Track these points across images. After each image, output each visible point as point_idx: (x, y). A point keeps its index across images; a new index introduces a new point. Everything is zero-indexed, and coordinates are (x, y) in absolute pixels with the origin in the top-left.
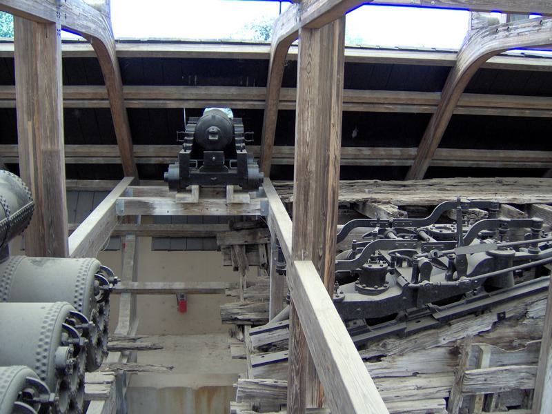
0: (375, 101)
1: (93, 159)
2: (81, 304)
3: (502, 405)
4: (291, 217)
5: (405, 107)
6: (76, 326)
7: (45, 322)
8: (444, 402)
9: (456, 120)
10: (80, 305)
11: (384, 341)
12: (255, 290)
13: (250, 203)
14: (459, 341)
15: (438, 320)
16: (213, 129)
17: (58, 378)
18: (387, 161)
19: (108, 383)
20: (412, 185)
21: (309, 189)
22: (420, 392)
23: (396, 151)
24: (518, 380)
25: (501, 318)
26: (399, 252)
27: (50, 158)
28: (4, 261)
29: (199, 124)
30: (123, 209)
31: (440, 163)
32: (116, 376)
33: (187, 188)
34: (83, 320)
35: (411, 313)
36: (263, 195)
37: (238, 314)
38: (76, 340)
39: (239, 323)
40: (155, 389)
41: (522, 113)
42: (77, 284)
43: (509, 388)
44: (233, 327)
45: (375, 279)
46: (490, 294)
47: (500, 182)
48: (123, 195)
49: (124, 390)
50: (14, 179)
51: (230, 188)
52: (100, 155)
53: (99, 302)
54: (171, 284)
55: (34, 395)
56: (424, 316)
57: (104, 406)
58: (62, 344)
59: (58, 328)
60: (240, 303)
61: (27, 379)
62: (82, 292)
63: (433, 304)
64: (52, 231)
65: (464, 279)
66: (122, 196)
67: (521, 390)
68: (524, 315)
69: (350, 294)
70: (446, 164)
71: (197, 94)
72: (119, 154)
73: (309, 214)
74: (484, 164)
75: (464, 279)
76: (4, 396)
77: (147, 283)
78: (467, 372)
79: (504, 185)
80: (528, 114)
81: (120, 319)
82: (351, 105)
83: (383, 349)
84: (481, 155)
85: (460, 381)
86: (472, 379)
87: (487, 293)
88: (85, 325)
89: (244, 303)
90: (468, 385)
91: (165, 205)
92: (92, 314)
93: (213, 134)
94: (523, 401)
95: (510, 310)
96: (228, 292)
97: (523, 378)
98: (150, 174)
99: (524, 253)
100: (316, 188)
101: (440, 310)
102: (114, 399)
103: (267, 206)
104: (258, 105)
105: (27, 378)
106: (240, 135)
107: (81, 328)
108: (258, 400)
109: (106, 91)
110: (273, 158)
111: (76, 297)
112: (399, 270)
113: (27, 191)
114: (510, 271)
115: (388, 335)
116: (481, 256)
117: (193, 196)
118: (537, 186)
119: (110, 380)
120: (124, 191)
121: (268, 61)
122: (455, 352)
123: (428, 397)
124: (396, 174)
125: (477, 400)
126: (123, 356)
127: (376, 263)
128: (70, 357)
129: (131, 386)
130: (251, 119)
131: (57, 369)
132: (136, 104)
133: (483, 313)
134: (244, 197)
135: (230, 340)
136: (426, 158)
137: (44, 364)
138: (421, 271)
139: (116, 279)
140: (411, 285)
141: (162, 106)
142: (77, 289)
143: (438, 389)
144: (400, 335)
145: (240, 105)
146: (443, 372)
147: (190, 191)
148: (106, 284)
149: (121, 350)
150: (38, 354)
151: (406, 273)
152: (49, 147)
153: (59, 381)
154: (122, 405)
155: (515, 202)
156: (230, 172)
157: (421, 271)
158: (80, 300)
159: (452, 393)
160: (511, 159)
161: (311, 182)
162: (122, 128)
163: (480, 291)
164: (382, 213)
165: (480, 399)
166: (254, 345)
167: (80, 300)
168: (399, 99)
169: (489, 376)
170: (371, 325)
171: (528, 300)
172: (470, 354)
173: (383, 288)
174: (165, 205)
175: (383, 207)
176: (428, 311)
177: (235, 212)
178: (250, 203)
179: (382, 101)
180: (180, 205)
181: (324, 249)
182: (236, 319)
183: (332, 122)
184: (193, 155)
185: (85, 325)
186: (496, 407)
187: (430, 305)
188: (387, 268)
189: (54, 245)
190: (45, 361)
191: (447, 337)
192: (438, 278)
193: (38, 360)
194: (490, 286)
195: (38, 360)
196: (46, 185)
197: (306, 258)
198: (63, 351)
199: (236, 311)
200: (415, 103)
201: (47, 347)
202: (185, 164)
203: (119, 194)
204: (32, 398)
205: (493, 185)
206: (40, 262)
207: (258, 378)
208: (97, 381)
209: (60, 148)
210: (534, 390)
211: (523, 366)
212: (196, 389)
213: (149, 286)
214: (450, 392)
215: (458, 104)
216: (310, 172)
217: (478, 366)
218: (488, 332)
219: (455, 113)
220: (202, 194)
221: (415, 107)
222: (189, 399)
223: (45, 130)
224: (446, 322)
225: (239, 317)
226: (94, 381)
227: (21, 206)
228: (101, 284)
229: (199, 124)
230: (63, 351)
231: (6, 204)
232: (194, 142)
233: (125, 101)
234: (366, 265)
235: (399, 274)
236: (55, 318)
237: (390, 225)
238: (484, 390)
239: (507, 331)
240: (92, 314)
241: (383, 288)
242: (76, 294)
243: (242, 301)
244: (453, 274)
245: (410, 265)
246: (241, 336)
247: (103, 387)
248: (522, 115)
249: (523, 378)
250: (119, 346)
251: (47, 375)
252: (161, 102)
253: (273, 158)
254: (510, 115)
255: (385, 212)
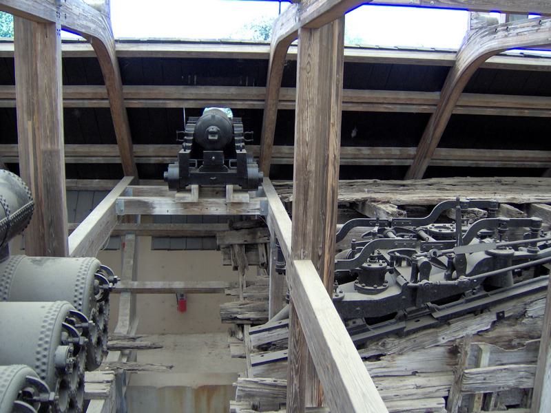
0: (375, 101)
1: (93, 159)
2: (81, 303)
3: (501, 404)
4: (291, 217)
5: (404, 106)
6: (76, 325)
7: (45, 321)
8: (443, 401)
9: (455, 120)
10: (80, 305)
11: (383, 340)
12: (255, 289)
13: (250, 203)
14: (458, 340)
15: (437, 319)
16: (213, 129)
17: (58, 377)
18: (386, 160)
19: (108, 382)
20: (412, 185)
21: (308, 188)
22: (420, 391)
23: (395, 151)
24: (517, 379)
25: (500, 317)
26: (398, 252)
27: (50, 157)
28: (4, 261)
29: (199, 123)
30: (123, 208)
31: (439, 163)
32: (116, 375)
33: (187, 187)
34: (83, 320)
35: (410, 312)
36: (263, 194)
37: (237, 313)
38: (76, 339)
39: (239, 322)
40: (155, 388)
41: (521, 113)
42: (77, 283)
43: (508, 387)
44: (233, 326)
45: (374, 278)
46: (489, 293)
47: (499, 182)
48: (123, 194)
49: (124, 389)
50: (14, 178)
51: (229, 187)
52: (99, 154)
53: (99, 301)
54: (171, 283)
55: (34, 394)
56: (424, 316)
57: (104, 405)
58: (62, 344)
59: (58, 327)
60: (240, 302)
61: (27, 378)
62: (81, 291)
63: (432, 303)
64: (52, 230)
65: (463, 278)
66: (121, 195)
67: (521, 389)
68: (523, 315)
69: (350, 293)
70: (446, 164)
71: (197, 94)
72: (118, 154)
73: (308, 214)
74: (483, 164)
75: (463, 278)
76: (4, 395)
77: (147, 283)
78: (466, 371)
79: (503, 184)
80: (527, 113)
81: (120, 318)
82: (350, 105)
83: (382, 348)
84: (480, 154)
85: (459, 380)
86: (471, 379)
87: (486, 293)
88: (85, 325)
89: (244, 302)
90: (467, 384)
91: (164, 204)
92: (92, 313)
93: (213, 133)
94: (522, 400)
95: (509, 309)
96: (227, 292)
97: (522, 378)
98: (150, 173)
99: (523, 252)
100: (316, 187)
101: (439, 310)
102: (114, 398)
103: (266, 205)
104: (257, 105)
105: (27, 377)
106: (239, 135)
107: (81, 327)
108: (258, 399)
109: (106, 91)
110: (273, 157)
111: (76, 296)
112: (399, 269)
113: (27, 191)
114: (509, 270)
115: (387, 334)
116: (480, 256)
117: (192, 195)
118: (536, 186)
119: (109, 379)
120: (124, 191)
121: (267, 61)
122: (454, 351)
123: (427, 396)
124: (395, 173)
125: (476, 399)
126: (123, 355)
127: (376, 262)
128: (70, 357)
129: (130, 385)
130: (251, 118)
131: (57, 368)
132: (136, 104)
133: (482, 312)
134: (244, 197)
135: (230, 340)
136: (425, 157)
137: (44, 364)
138: (420, 271)
139: (115, 279)
140: (411, 284)
141: (162, 106)
142: (77, 288)
143: (437, 388)
144: (399, 334)
145: (240, 105)
146: (442, 372)
147: (190, 191)
148: (106, 283)
149: (121, 349)
150: (38, 353)
151: (405, 273)
152: (49, 146)
153: (59, 380)
154: (121, 404)
155: (515, 202)
156: (230, 171)
157: (420, 271)
158: (80, 299)
159: (451, 393)
160: (510, 159)
161: (310, 181)
162: (121, 128)
163: (479, 290)
164: (381, 212)
165: (479, 398)
166: (253, 344)
167: (80, 299)
168: (398, 99)
169: (488, 375)
170: (370, 324)
171: (527, 299)
172: (469, 353)
173: (382, 287)
174: (164, 204)
175: (382, 206)
176: (427, 310)
177: (234, 212)
178: (250, 203)
179: (381, 101)
180: (179, 204)
181: (323, 248)
182: (236, 318)
183: (332, 121)
184: (192, 155)
185: (85, 325)
186: (495, 406)
187: (429, 304)
188: (386, 267)
189: (54, 245)
190: (45, 360)
191: (446, 336)
192: (437, 277)
193: (38, 360)
194: (490, 285)
195: (38, 360)
196: (46, 185)
197: (305, 257)
198: (63, 350)
199: (235, 310)
200: (415, 102)
201: (46, 346)
202: (184, 164)
203: (119, 194)
204: (32, 397)
205: (492, 185)
206: (40, 261)
207: (258, 377)
208: (97, 380)
209: (60, 147)
210: (533, 389)
211: (522, 366)
212: (196, 388)
213: (149, 285)
214: (449, 391)
215: (457, 104)
216: (310, 172)
217: (477, 365)
218: (487, 331)
219: (454, 113)
220: (201, 194)
221: (414, 107)
222: (189, 398)
223: (45, 130)
224: (446, 321)
225: (239, 316)
226: (93, 380)
227: (21, 205)
228: (101, 284)
229: (199, 123)
230: (63, 350)
231: (6, 204)
232: (194, 141)
233: (125, 101)
234: (365, 265)
235: (398, 274)
236: (55, 317)
237: (390, 224)
238: (483, 389)
239: (506, 330)
240: (92, 313)
241: (382, 287)
242: (76, 294)
243: (242, 301)
244: (452, 273)
245: (409, 265)
246: (240, 335)
247: (103, 386)
248: (521, 115)
249: (522, 378)
250: (119, 345)
251: (47, 374)
252: (161, 101)
253: (273, 157)
254: (509, 115)
255: (384, 211)
